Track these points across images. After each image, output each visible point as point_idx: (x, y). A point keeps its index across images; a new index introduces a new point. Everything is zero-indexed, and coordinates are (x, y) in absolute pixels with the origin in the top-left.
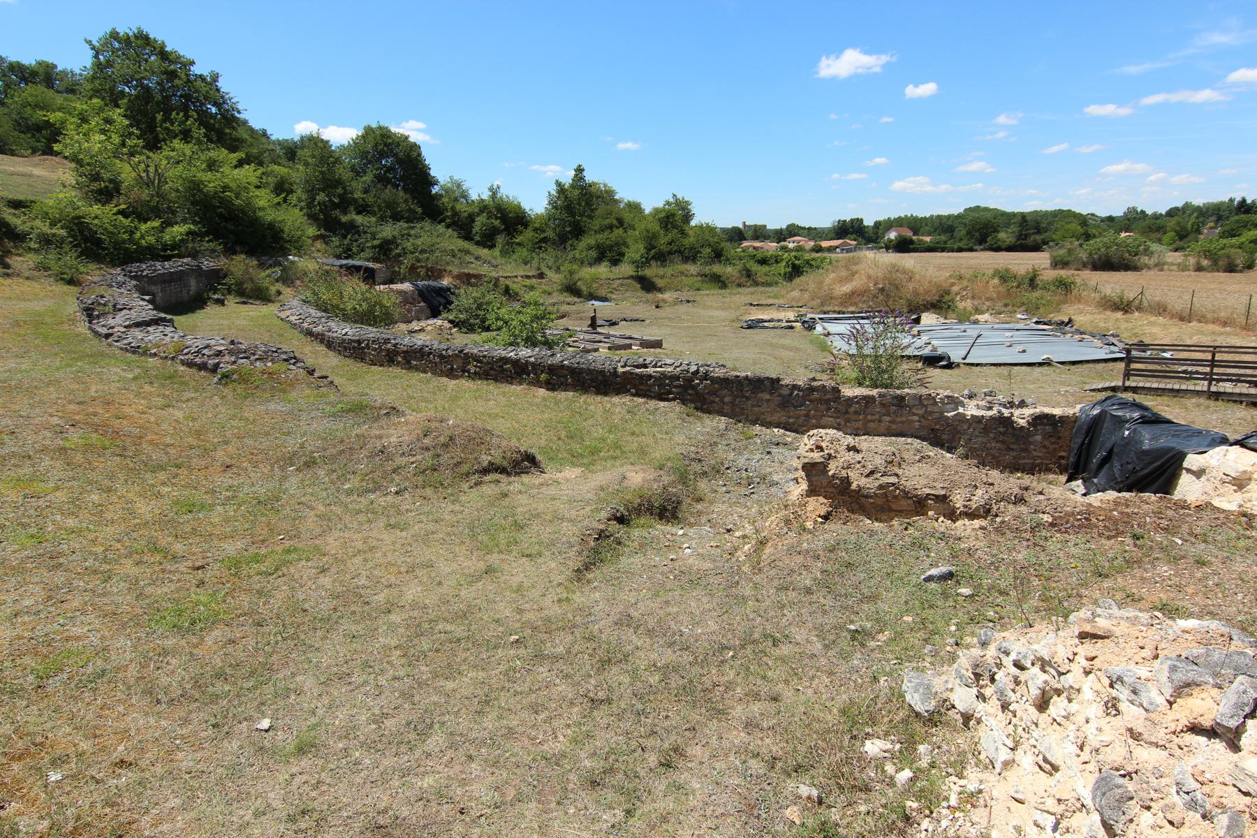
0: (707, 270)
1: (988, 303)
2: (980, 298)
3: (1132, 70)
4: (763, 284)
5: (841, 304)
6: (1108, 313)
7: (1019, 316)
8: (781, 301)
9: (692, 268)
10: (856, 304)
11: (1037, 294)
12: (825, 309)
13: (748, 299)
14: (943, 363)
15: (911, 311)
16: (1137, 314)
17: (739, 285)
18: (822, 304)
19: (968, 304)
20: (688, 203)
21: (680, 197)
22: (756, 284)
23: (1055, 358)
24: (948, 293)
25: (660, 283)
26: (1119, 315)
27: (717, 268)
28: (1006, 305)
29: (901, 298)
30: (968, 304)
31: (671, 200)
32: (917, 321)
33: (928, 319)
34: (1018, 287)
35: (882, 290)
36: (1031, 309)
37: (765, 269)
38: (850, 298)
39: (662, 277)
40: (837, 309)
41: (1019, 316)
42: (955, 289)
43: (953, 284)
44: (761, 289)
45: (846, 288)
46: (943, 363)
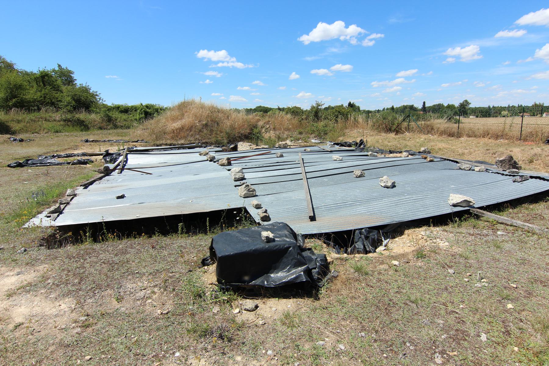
0: (69, 116)
1: (286, 133)
2: (280, 129)
3: (309, 59)
4: (122, 127)
5: (172, 138)
6: (383, 134)
7: (313, 141)
8: (127, 139)
9: (57, 116)
10: (185, 137)
11: (321, 124)
12: (158, 143)
13: (84, 138)
14: (281, 276)
15: (230, 142)
16: (407, 134)
17: (101, 128)
18: (157, 139)
19: (272, 134)
20: (70, 72)
21: (64, 66)
22: (116, 127)
23: (479, 200)
24: (255, 127)
25: (15, 126)
26: (392, 135)
27: (82, 115)
28: (301, 133)
29: (221, 132)
30: (272, 134)
31: (57, 69)
32: (235, 149)
33: (243, 146)
34: (306, 119)
35: (206, 125)
36: (322, 135)
37: (124, 116)
38: (178, 133)
39: (19, 122)
40: (169, 142)
41: (313, 141)
42: (261, 123)
43: (258, 120)
44: (119, 131)
45: (177, 125)
46: (281, 276)
